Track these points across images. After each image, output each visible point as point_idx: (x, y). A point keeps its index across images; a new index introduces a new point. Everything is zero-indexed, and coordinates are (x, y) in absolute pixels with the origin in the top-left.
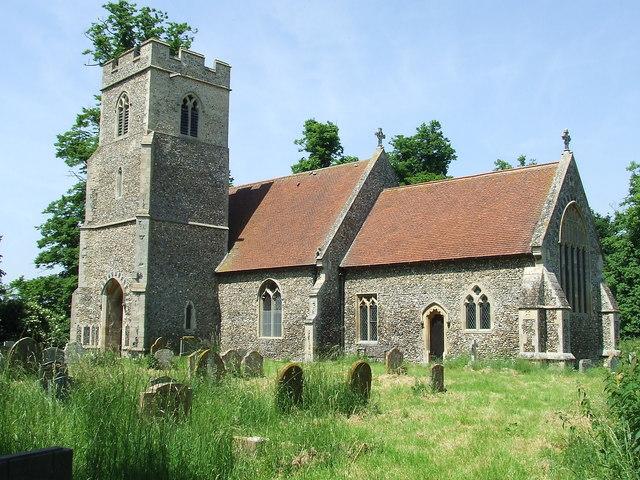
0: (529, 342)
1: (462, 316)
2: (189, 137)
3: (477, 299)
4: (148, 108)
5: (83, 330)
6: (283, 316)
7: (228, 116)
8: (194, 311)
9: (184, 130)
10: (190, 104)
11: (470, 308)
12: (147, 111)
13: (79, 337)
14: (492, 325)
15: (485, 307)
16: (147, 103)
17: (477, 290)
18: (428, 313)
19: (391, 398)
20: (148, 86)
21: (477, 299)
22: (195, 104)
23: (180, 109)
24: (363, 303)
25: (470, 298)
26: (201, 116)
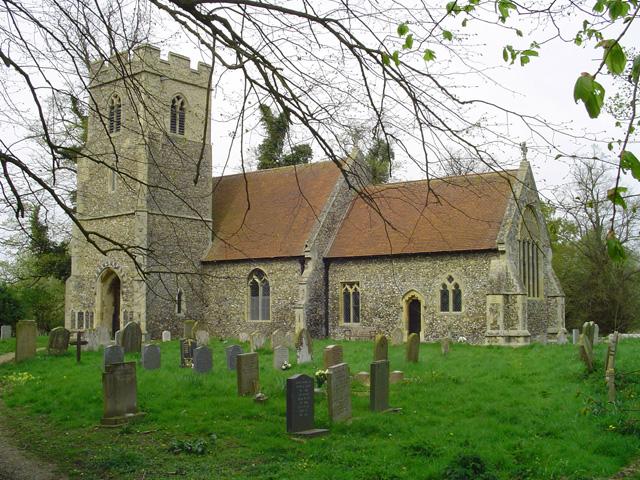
3: (450, 287)
5: (77, 315)
9: (173, 128)
10: (178, 103)
11: (444, 294)
13: (73, 321)
14: (463, 309)
15: (457, 293)
17: (450, 279)
21: (450, 287)
22: (182, 103)
25: (444, 286)
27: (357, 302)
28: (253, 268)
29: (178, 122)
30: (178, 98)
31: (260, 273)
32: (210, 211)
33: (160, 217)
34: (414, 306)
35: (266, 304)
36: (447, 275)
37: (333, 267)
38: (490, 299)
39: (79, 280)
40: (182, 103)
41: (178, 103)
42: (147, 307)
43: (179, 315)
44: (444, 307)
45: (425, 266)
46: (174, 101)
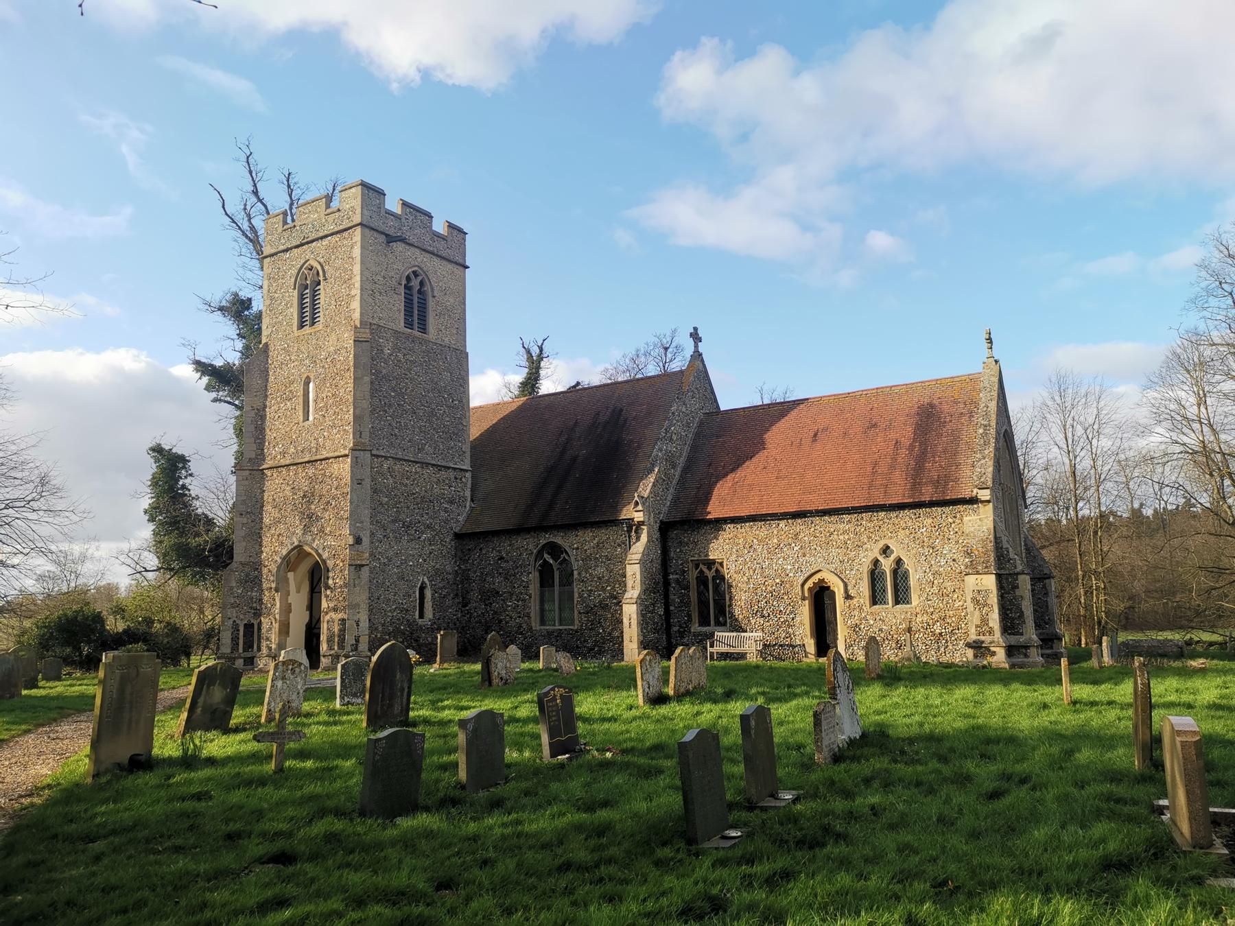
0: (984, 621)
1: (864, 588)
2: (416, 333)
3: (887, 565)
4: (358, 285)
5: (242, 629)
6: (576, 595)
7: (464, 304)
8: (428, 593)
9: (409, 324)
10: (415, 283)
11: (875, 576)
12: (356, 291)
13: (235, 640)
14: (915, 600)
15: (899, 571)
16: (357, 279)
17: (886, 551)
18: (809, 584)
19: (41, 796)
20: (357, 252)
21: (887, 565)
22: (422, 284)
23: (402, 290)
24: (702, 571)
25: (876, 562)
26: (431, 304)
27: (1040, 578)
28: (543, 542)
29: (416, 300)
30: (415, 274)
31: (555, 550)
32: (468, 454)
33: (391, 462)
34: (821, 599)
35: (567, 598)
36: (881, 544)
37: (673, 534)
38: (971, 580)
39: (247, 569)
40: (422, 284)
41: (415, 283)
42: (370, 610)
43: (420, 622)
44: (876, 598)
45: (842, 527)
46: (408, 279)
